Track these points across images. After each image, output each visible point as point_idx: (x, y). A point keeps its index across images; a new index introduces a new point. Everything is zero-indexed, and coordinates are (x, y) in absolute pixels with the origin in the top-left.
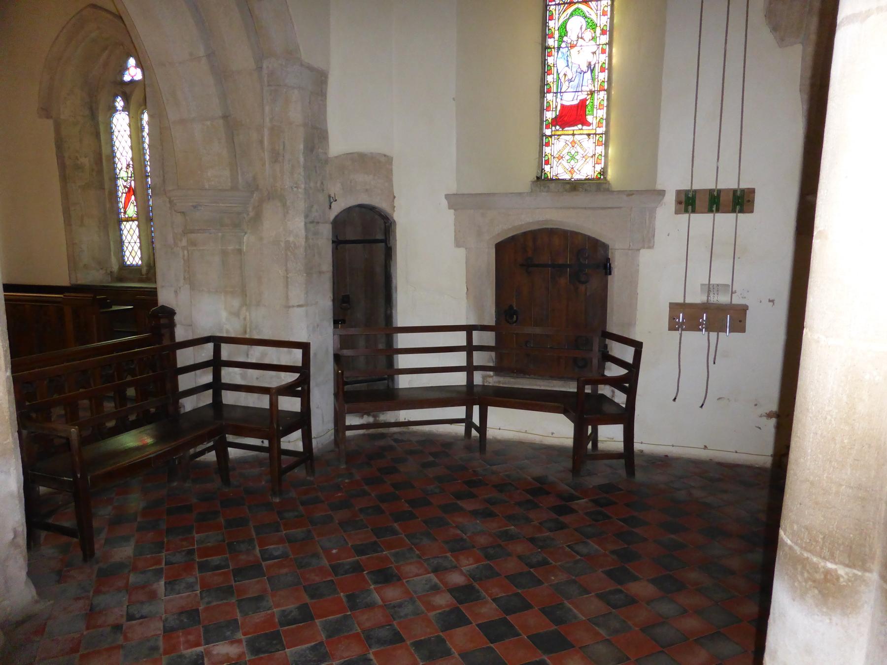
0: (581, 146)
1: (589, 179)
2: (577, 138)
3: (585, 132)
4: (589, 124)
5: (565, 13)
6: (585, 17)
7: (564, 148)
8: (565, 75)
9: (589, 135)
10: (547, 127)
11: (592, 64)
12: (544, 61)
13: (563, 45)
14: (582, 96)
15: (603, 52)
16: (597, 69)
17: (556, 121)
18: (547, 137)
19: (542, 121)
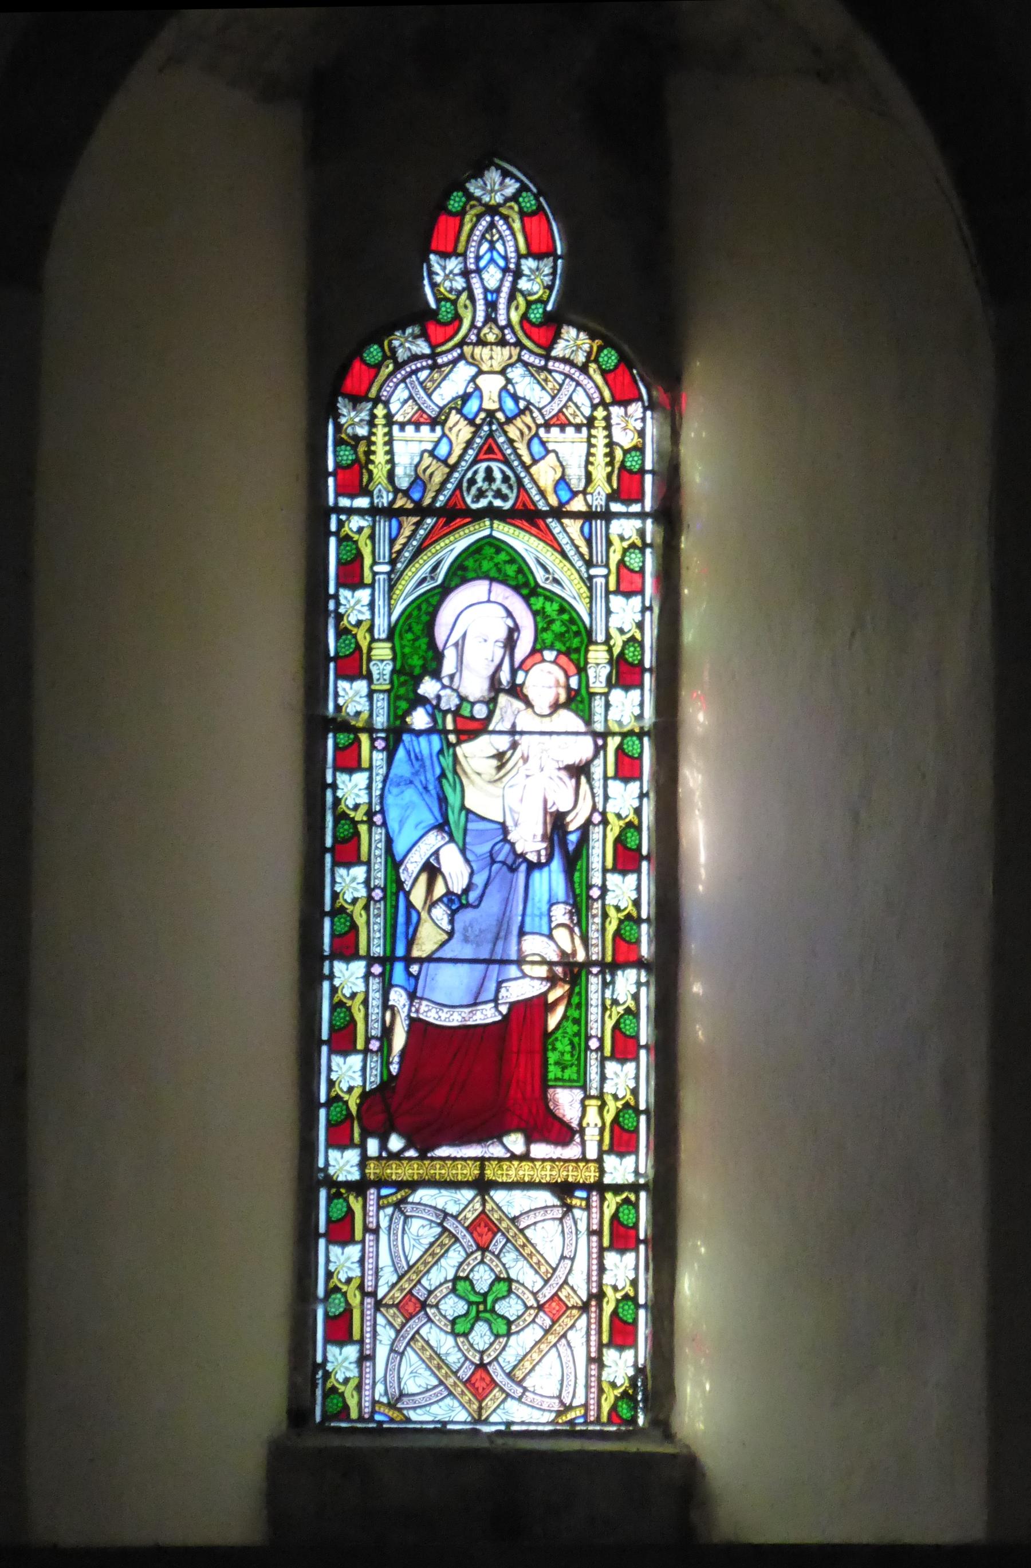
0: (527, 1251)
1: (572, 1433)
2: (510, 1202)
3: (547, 1174)
4: (561, 1132)
5: (423, 566)
6: (527, 589)
7: (433, 1254)
8: (432, 870)
9: (563, 1190)
10: (340, 1140)
11: (574, 822)
12: (315, 791)
13: (420, 719)
14: (521, 989)
15: (627, 769)
16: (600, 852)
17: (380, 1110)
18: (338, 1189)
19: (308, 1105)
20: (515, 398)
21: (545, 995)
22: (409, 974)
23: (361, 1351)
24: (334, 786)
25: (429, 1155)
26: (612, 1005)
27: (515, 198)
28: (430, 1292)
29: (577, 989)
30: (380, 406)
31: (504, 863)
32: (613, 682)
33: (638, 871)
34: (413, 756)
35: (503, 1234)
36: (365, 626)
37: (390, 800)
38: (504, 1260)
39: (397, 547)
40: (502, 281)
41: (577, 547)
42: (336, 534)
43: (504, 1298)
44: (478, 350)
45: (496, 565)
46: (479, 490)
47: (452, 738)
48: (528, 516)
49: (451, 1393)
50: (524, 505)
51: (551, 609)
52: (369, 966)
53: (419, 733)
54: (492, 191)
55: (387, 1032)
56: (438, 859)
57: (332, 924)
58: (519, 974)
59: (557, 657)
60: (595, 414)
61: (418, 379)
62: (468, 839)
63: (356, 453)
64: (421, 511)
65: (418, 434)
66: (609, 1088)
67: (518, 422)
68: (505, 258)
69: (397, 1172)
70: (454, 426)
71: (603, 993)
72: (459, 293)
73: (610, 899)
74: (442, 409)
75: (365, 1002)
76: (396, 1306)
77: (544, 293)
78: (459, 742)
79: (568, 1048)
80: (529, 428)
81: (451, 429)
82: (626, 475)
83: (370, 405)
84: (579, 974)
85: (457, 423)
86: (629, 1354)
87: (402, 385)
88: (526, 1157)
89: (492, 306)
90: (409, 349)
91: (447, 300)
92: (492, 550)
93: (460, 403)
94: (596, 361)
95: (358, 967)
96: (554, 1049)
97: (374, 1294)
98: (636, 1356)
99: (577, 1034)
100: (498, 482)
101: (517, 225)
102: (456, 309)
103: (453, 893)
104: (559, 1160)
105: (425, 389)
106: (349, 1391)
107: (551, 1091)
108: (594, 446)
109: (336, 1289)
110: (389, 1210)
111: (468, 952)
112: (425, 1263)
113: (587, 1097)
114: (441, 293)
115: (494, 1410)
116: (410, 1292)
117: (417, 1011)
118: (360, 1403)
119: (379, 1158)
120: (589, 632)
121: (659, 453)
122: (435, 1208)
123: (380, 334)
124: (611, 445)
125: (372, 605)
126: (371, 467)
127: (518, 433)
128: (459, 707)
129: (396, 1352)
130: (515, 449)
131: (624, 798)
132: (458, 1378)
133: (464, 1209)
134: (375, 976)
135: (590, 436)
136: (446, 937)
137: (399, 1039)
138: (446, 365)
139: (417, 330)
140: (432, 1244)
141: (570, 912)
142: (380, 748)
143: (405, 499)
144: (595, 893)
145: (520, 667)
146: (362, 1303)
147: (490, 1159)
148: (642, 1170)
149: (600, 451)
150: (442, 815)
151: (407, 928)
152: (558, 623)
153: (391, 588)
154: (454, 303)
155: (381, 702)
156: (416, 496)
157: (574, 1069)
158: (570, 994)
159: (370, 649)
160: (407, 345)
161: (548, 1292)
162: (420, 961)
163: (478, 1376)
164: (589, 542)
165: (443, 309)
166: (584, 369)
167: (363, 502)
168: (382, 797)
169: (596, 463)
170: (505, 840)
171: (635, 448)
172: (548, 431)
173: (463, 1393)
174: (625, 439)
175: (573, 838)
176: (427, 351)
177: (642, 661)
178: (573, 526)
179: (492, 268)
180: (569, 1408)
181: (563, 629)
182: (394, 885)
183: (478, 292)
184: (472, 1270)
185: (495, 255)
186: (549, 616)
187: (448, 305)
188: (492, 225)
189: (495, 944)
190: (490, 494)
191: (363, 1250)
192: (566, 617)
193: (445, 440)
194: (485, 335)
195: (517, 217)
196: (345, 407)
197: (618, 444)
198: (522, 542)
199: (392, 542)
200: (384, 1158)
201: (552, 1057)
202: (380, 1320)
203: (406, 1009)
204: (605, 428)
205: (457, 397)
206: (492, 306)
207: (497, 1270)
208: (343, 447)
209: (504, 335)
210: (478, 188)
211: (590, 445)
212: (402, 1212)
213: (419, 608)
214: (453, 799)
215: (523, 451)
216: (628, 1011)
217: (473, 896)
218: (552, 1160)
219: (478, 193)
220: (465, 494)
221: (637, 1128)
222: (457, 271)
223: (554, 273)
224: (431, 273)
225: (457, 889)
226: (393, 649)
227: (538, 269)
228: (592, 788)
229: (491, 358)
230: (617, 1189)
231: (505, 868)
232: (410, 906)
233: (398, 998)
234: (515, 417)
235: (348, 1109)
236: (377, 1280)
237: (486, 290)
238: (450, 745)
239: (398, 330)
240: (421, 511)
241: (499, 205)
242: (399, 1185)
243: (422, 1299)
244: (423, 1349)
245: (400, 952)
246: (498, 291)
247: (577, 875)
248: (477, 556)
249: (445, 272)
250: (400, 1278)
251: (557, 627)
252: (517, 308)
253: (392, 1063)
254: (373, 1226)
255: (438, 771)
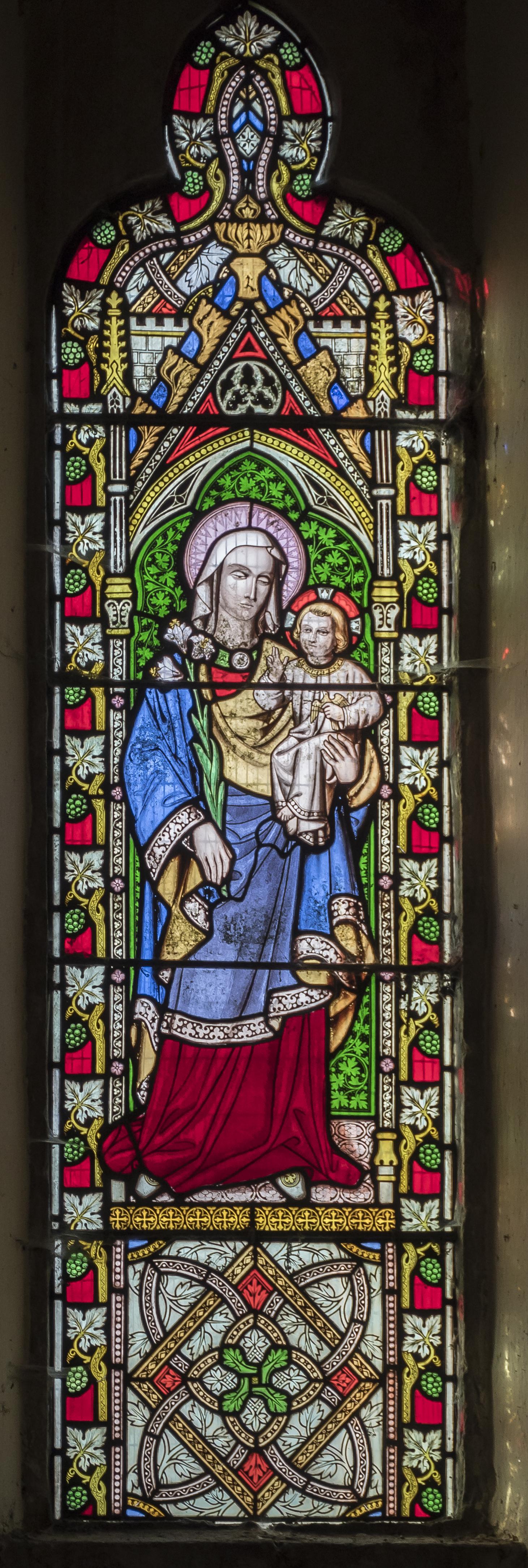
1: (365, 1524)
4: (351, 1173)
6: (298, 515)
7: (195, 1319)
8: (184, 854)
13: (166, 670)
15: (423, 733)
17: (127, 1147)
20: (279, 285)
21: (327, 1004)
22: (159, 982)
23: (109, 1434)
24: (63, 753)
25: (187, 1200)
26: (408, 1019)
27: (274, 48)
28: (192, 1364)
29: (366, 1000)
30: (114, 295)
31: (273, 846)
32: (405, 626)
33: (439, 856)
34: (158, 717)
35: (280, 1294)
36: (98, 558)
37: (131, 770)
38: (282, 1324)
39: (137, 462)
40: (260, 146)
41: (356, 463)
42: (62, 448)
43: (282, 1369)
44: (232, 229)
45: (258, 483)
46: (237, 393)
47: (206, 693)
48: (297, 425)
49: (219, 1484)
50: (292, 411)
51: (327, 537)
52: (108, 974)
53: (165, 687)
54: (247, 40)
55: (133, 1052)
56: (192, 842)
57: (63, 921)
58: (293, 982)
59: (333, 595)
60: (376, 304)
61: (159, 262)
62: (228, 818)
63: (85, 350)
64: (164, 419)
65: (159, 328)
66: (406, 1119)
67: (283, 314)
68: (264, 120)
69: (145, 1220)
70: (204, 318)
71: (398, 1004)
72: (209, 161)
73: (405, 890)
74: (189, 298)
75: (105, 1017)
76: (151, 1380)
77: (312, 161)
78: (216, 699)
79: (356, 1071)
80: (296, 322)
81: (200, 322)
82: (413, 376)
83: (101, 293)
84: (368, 982)
85: (209, 314)
86: (434, 1436)
87: (141, 270)
88: (306, 1202)
89: (249, 176)
90: (149, 227)
91: (194, 169)
92: (254, 466)
93: (211, 290)
94: (376, 242)
95: (96, 973)
96: (338, 1072)
97: (123, 1367)
98: (443, 1438)
99: (366, 1054)
100: (259, 384)
101: (277, 81)
102: (205, 180)
103: (211, 884)
104: (346, 1205)
105: (167, 275)
106: (94, 1481)
107: (335, 1123)
108: (376, 342)
109: (77, 1361)
110: (139, 1267)
111: (229, 954)
112: (185, 1329)
113: (379, 1129)
114: (187, 161)
115: (272, 1504)
116: (167, 1363)
117: (169, 1027)
118: (108, 1497)
119: (126, 1204)
120: (374, 566)
121: (456, 352)
122: (196, 1263)
123: (114, 207)
124: (395, 340)
125: (106, 533)
126: (104, 366)
127: (282, 327)
128: (215, 656)
129: (151, 1435)
130: (279, 346)
131: (417, 767)
132: (228, 1465)
133: (231, 1264)
134: (116, 985)
135: (370, 330)
136: (202, 936)
137: (148, 1063)
138: (195, 245)
139: (158, 205)
140: (193, 1306)
141: (356, 906)
142: (118, 706)
143: (145, 406)
144: (386, 882)
145: (289, 608)
146: (108, 1378)
147: (261, 1205)
148: (448, 1216)
149: (383, 347)
150: (195, 788)
151: (155, 927)
152: (336, 554)
153: (130, 512)
154: (203, 172)
155: (117, 650)
156: (160, 402)
157: (363, 1096)
158: (357, 1004)
159: (104, 586)
160: (146, 222)
161: (337, 1361)
162: (173, 965)
163: (252, 1462)
164: (371, 457)
165: (190, 180)
166: (361, 252)
167: (94, 408)
168: (121, 765)
169: (378, 363)
170: (274, 818)
171: (425, 345)
172: (319, 325)
173: (234, 1484)
174: (412, 335)
175: (358, 816)
176: (171, 229)
177: (439, 600)
178: (352, 440)
179: (248, 133)
180: (365, 1500)
181: (341, 561)
182: (138, 873)
183: (232, 159)
184: (242, 1337)
185: (250, 120)
186: (323, 546)
187: (196, 174)
188: (247, 81)
189: (264, 945)
190: (249, 398)
191: (108, 1315)
192: (344, 546)
193: (193, 335)
194: (240, 210)
195: (276, 70)
196: (71, 295)
197: (404, 340)
198: (288, 455)
199: (130, 457)
200: (132, 1204)
201: (337, 1081)
202: (132, 1397)
203: (155, 1025)
204: (387, 321)
205: (207, 285)
206: (249, 176)
207: (273, 1336)
208: (69, 344)
209: (264, 211)
210: (229, 36)
211: (371, 342)
212: (156, 1269)
213: (165, 535)
214: (211, 768)
215: (289, 347)
216: (429, 1025)
217: (235, 886)
218: (336, 1205)
219: (231, 42)
220: (219, 398)
221: (441, 1166)
222: (205, 135)
223: (323, 138)
224: (174, 137)
225: (216, 875)
226: (133, 586)
227: (303, 132)
228: (379, 754)
229: (249, 237)
230: (418, 1239)
231: (274, 852)
232: (158, 898)
233: (145, 1011)
234: (278, 308)
235: (87, 1144)
236: (126, 1350)
237: (240, 157)
238: (203, 701)
239: (133, 204)
240: (164, 419)
241: (256, 57)
242: (151, 1236)
243: (183, 1371)
244: (184, 1431)
245: (147, 955)
246: (256, 158)
247: (363, 860)
248: (234, 473)
249: (190, 135)
250: (154, 1347)
251: (335, 559)
252: (279, 179)
253: (140, 1090)
254: (120, 1285)
255: (190, 734)
